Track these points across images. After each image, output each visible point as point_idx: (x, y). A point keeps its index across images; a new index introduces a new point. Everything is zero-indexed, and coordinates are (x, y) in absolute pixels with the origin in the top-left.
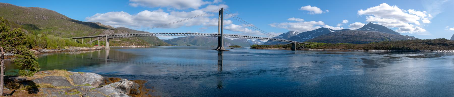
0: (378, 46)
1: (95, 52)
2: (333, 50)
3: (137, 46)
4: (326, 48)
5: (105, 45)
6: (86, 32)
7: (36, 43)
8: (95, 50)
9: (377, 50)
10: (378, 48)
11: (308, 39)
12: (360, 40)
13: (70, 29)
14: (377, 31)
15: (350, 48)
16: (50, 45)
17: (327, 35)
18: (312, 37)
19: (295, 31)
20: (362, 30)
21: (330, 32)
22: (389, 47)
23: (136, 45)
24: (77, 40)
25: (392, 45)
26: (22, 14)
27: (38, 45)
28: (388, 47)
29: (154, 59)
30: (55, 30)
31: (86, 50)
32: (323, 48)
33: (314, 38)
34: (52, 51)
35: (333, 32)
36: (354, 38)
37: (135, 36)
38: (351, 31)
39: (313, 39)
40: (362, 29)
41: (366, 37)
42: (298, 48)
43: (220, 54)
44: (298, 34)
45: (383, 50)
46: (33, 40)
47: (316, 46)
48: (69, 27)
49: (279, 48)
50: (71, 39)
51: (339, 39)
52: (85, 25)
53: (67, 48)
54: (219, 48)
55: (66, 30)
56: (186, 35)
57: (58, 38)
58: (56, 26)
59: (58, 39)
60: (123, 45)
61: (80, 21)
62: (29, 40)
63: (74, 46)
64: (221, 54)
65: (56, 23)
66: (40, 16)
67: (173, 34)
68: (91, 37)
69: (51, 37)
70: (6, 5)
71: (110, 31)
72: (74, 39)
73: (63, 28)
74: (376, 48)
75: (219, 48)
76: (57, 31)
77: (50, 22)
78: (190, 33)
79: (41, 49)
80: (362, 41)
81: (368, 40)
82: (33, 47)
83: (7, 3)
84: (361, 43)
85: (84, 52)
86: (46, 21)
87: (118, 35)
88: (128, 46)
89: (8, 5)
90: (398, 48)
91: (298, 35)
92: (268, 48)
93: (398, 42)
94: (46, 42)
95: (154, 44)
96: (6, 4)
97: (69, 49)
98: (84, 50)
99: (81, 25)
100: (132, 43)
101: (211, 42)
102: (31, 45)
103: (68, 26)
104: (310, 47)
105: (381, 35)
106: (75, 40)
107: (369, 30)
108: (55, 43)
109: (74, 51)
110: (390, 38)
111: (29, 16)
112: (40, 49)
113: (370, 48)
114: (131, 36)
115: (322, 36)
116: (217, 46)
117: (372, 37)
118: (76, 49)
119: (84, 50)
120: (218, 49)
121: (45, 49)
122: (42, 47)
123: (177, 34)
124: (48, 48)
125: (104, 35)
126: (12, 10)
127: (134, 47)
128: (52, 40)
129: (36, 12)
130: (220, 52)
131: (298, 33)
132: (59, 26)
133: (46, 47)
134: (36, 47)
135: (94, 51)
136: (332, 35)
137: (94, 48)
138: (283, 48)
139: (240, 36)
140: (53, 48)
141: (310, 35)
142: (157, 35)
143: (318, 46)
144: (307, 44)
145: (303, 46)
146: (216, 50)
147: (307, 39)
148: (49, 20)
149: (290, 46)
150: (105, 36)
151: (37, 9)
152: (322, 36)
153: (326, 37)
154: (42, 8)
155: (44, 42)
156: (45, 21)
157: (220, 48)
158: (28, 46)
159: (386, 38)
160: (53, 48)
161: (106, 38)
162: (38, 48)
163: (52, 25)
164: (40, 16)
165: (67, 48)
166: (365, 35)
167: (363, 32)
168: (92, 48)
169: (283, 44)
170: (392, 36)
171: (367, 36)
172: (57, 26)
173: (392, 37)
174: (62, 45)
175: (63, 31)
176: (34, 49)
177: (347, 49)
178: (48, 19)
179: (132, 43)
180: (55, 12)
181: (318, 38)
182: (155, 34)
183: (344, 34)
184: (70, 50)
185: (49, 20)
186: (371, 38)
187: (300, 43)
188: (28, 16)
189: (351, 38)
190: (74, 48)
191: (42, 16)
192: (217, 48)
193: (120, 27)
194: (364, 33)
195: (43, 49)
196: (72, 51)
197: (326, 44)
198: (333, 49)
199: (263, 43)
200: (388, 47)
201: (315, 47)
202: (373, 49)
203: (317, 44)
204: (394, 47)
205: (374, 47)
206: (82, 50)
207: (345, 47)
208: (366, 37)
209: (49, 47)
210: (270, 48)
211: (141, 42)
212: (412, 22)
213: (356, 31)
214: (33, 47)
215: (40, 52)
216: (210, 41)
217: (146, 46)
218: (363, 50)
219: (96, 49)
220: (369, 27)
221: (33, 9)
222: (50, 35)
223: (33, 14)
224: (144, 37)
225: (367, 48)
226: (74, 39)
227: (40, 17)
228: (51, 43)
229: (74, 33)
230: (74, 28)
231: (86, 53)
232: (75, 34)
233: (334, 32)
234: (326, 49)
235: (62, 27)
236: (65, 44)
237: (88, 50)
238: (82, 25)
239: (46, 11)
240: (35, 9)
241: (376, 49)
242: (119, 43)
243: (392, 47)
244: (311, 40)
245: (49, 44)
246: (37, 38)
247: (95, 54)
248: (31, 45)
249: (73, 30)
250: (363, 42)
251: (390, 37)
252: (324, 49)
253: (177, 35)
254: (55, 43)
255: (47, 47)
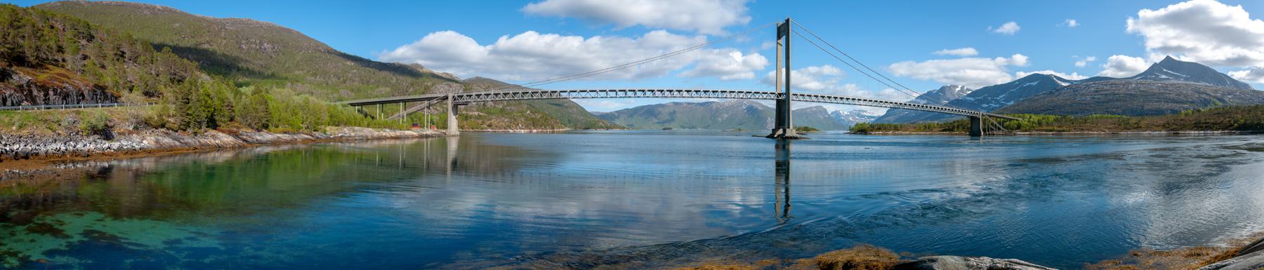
0: (1204, 121)
1: (416, 145)
2: (1083, 134)
3: (530, 129)
4: (1064, 128)
5: (445, 127)
6: (383, 89)
7: (233, 111)
8: (417, 137)
9: (1202, 132)
10: (1204, 125)
11: (997, 108)
12: (1142, 106)
13: (339, 79)
14: (1186, 79)
15: (1128, 126)
16: (279, 120)
17: (1051, 93)
18: (1008, 100)
19: (960, 86)
20: (1146, 78)
21: (1058, 85)
22: (1235, 122)
23: (527, 127)
24: (360, 107)
25: (1242, 116)
26: (204, 35)
27: (237, 118)
28: (1232, 122)
29: (571, 167)
30: (297, 81)
31: (392, 138)
32: (1055, 128)
33: (1012, 103)
34: (286, 138)
35: (1065, 87)
36: (1126, 101)
37: (528, 96)
38: (1117, 82)
39: (1013, 105)
40: (1145, 75)
41: (1158, 97)
42: (988, 131)
43: (784, 147)
44: (969, 92)
45: (1217, 129)
46: (224, 102)
47: (1033, 123)
48: (336, 75)
49: (931, 130)
50: (344, 106)
51: (1085, 104)
52: (380, 70)
53: (332, 131)
54: (780, 132)
55: (327, 84)
56: (661, 95)
57: (307, 98)
58: (299, 70)
59: (307, 102)
60: (490, 126)
61: (367, 58)
62: (207, 98)
63: (355, 125)
64: (787, 147)
65: (298, 62)
66: (255, 43)
67: (620, 91)
68: (405, 101)
69: (283, 94)
70: (159, 10)
71: (451, 86)
72: (353, 105)
73: (318, 77)
74: (1198, 126)
75: (780, 132)
76: (303, 84)
77: (283, 62)
78: (671, 89)
79: (250, 130)
80: (1149, 110)
81: (1164, 106)
82: (222, 125)
83: (164, 5)
84: (1147, 115)
85: (384, 142)
86: (271, 57)
87: (485, 93)
88: (505, 128)
89: (165, 10)
90: (1259, 124)
91: (969, 95)
92: (900, 132)
93: (1257, 107)
94: (267, 111)
95: (572, 124)
96: (160, 8)
97: (340, 135)
98: (385, 136)
99: (370, 71)
100: (515, 119)
101: (727, 118)
102: (212, 115)
103: (333, 70)
104: (1019, 127)
105: (1199, 92)
106: (357, 107)
107: (1164, 77)
108: (296, 114)
109: (356, 140)
110: (1226, 99)
111: (224, 42)
112: (244, 130)
113: (1184, 127)
114: (516, 98)
115: (1036, 98)
116: (774, 128)
117: (1176, 97)
118: (361, 134)
119: (386, 138)
120: (775, 136)
121: (261, 133)
122: (253, 125)
123: (634, 91)
124: (273, 128)
125: (442, 95)
126: (178, 25)
127: (523, 131)
128: (284, 104)
129: (243, 30)
130: (783, 142)
131: (968, 90)
132: (308, 72)
133: (266, 127)
134: (231, 124)
135: (415, 140)
136: (1065, 93)
137: (414, 133)
138: (944, 131)
139: (803, 95)
140: (289, 129)
141: (1001, 96)
142: (574, 94)
143: (1040, 123)
144: (1010, 120)
145: (1000, 123)
146: (771, 136)
147: (994, 106)
148: (281, 54)
149: (962, 125)
150: (446, 98)
151: (247, 23)
152: (1036, 98)
153: (1047, 99)
154: (261, 21)
155: (261, 108)
156: (269, 58)
157: (785, 131)
158: (204, 119)
159: (1215, 100)
160: (289, 129)
161: (450, 101)
162: (238, 128)
163: (289, 67)
164: (255, 43)
165: (332, 131)
166: (1155, 91)
167: (1149, 84)
168: (407, 132)
169: (942, 121)
170: (1229, 94)
171: (1162, 93)
172: (302, 70)
173: (1230, 97)
174: (318, 119)
175: (319, 85)
176: (223, 132)
177: (1122, 130)
178: (276, 52)
179: (515, 119)
180: (299, 33)
181: (1026, 104)
182: (566, 92)
183: (1097, 92)
184: (342, 136)
185: (281, 54)
186: (1174, 101)
187: (993, 116)
188: (222, 42)
189: (1118, 100)
190: (354, 131)
191: (261, 44)
192: (774, 131)
193: (477, 78)
194: (1154, 88)
195: (257, 133)
196: (348, 140)
197: (1060, 117)
198: (1082, 130)
199: (873, 119)
200: (1232, 122)
201: (1033, 127)
202: (1191, 129)
203: (1035, 118)
204: (1248, 122)
205: (1193, 122)
206: (380, 138)
207: (1115, 124)
208: (1158, 98)
209: (277, 127)
210: (907, 133)
211: (538, 117)
212: (1205, 60)
213: (1130, 80)
214: (222, 125)
215: (244, 140)
216: (726, 116)
217: (553, 128)
218: (1164, 132)
219: (421, 137)
220: (1165, 70)
221: (234, 22)
222: (279, 90)
223: (234, 36)
224: (545, 102)
225: (1175, 126)
226: (353, 105)
227: (254, 46)
228: (284, 115)
229: (350, 93)
230: (351, 79)
231: (391, 147)
232: (353, 94)
233: (1069, 86)
234: (1064, 131)
235: (315, 75)
236: (327, 118)
237: (397, 138)
238: (371, 69)
239: (271, 28)
240: (241, 22)
241: (1201, 127)
242: (480, 121)
243: (1242, 121)
244: (1006, 108)
245: (276, 116)
246: (238, 96)
247: (416, 150)
248: (212, 115)
249: (348, 82)
250: (1153, 110)
251: (1224, 94)
252: (1060, 131)
253: (633, 95)
254: (296, 114)
255: (270, 127)
